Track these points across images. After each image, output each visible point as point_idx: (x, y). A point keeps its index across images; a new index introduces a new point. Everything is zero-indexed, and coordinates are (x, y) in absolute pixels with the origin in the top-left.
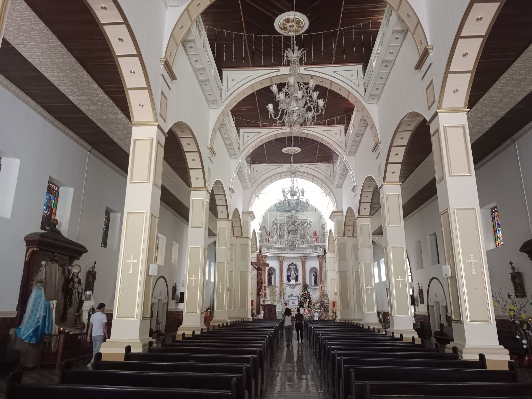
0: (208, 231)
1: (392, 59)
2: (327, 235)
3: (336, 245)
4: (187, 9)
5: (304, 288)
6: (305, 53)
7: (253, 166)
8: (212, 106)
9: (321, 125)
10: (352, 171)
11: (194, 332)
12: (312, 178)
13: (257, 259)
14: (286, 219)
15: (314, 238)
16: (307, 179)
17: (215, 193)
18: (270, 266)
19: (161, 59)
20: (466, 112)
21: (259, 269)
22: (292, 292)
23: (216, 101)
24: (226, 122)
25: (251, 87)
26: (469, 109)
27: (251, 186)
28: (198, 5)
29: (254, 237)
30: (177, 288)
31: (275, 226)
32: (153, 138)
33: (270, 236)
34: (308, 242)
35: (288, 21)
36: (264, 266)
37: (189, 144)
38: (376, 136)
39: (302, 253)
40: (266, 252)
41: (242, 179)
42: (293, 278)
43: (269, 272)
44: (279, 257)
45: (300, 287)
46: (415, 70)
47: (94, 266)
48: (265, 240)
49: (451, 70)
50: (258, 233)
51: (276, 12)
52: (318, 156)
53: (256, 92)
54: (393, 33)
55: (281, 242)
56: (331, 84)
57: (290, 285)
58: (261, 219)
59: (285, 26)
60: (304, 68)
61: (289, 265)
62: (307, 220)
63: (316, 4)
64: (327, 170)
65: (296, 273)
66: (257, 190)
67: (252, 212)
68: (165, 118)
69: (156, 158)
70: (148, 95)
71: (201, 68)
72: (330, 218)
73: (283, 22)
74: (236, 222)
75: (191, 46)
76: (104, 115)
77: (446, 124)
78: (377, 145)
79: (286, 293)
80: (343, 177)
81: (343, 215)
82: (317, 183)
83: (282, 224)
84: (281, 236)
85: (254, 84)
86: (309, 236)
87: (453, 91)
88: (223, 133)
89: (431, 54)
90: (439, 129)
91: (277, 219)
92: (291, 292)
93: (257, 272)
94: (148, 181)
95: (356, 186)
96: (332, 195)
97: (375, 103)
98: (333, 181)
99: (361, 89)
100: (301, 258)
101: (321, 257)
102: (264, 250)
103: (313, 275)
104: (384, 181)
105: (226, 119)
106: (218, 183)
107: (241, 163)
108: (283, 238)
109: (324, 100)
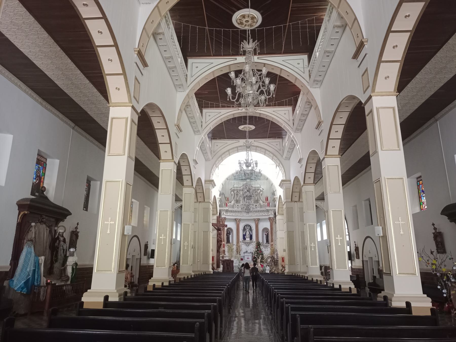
1: (333, 50)
2: (277, 200)
4: (157, 6)
5: (257, 246)
6: (259, 44)
7: (214, 141)
8: (179, 90)
9: (272, 106)
10: (299, 146)
11: (163, 283)
14: (242, 186)
15: (266, 203)
16: (260, 153)
18: (228, 227)
19: (135, 49)
20: (396, 95)
21: (219, 230)
23: (182, 85)
25: (212, 73)
28: (167, 3)
29: (215, 202)
30: (148, 246)
31: (232, 193)
33: (228, 201)
35: (244, 16)
37: (159, 122)
38: (319, 116)
39: (256, 215)
40: (224, 215)
42: (248, 237)
43: (227, 232)
44: (236, 219)
46: (352, 59)
47: (77, 227)
48: (224, 205)
50: (218, 198)
55: (238, 206)
57: (245, 243)
59: (242, 21)
60: (258, 58)
61: (245, 226)
62: (260, 187)
65: (251, 233)
66: (217, 162)
67: (213, 180)
68: (138, 100)
72: (280, 185)
73: (240, 18)
74: (199, 189)
77: (378, 106)
78: (319, 123)
79: (242, 250)
81: (290, 183)
82: (269, 156)
83: (239, 191)
86: (262, 201)
88: (188, 113)
89: (366, 46)
90: (373, 110)
91: (234, 186)
92: (246, 249)
93: (218, 232)
96: (281, 166)
98: (282, 154)
99: (306, 76)
102: (223, 213)
103: (265, 235)
105: (191, 101)
106: (184, 156)
107: (204, 138)
108: (240, 203)
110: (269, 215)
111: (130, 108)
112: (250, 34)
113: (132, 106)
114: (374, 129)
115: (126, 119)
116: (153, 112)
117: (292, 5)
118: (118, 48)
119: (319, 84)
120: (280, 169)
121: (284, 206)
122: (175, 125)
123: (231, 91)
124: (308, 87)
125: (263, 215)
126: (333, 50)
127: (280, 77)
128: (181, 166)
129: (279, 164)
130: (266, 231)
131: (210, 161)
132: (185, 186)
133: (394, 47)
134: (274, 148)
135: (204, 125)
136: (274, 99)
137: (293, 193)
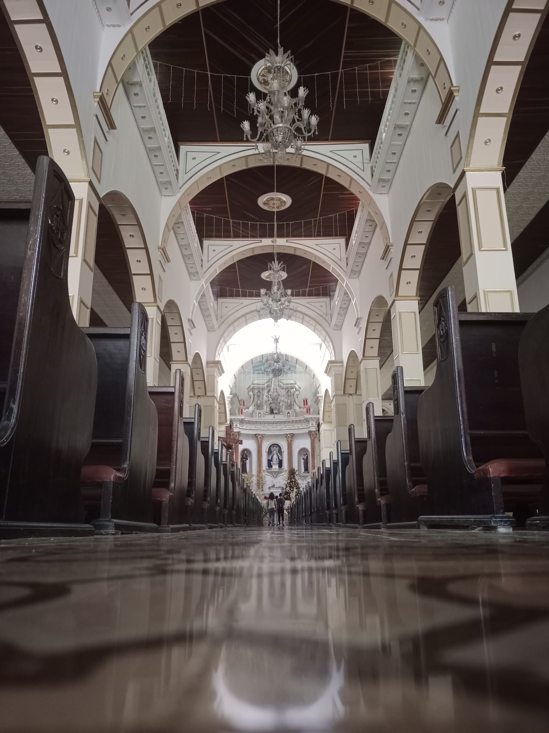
0: (158, 363)
1: (407, 123)
2: (321, 401)
3: (334, 406)
4: (130, 31)
6: (293, 58)
7: (221, 300)
8: (165, 192)
9: (314, 236)
12: (302, 318)
13: (227, 434)
14: (266, 382)
15: (305, 409)
17: (168, 323)
19: (94, 94)
20: (501, 170)
22: (274, 482)
23: (170, 183)
24: (184, 219)
25: (218, 168)
26: (504, 167)
27: (219, 327)
28: (146, 29)
29: (222, 403)
31: (251, 393)
32: (83, 198)
33: (244, 405)
34: (297, 415)
35: (272, 199)
36: (236, 443)
37: (133, 236)
40: (238, 428)
41: (206, 314)
42: (276, 463)
43: (242, 456)
44: (257, 434)
45: (285, 475)
46: (436, 125)
48: (237, 412)
49: (482, 111)
50: (228, 398)
51: (253, 56)
52: (309, 286)
53: (226, 179)
54: (409, 82)
56: (328, 168)
58: (233, 380)
59: (265, 78)
60: (287, 240)
61: (270, 446)
62: (296, 384)
63: (307, 46)
64: (321, 306)
65: (280, 457)
66: (227, 333)
67: (220, 361)
69: (84, 245)
70: (76, 136)
71: (150, 128)
73: (263, 72)
74: (198, 374)
75: (136, 92)
76: (11, 184)
77: (475, 186)
79: (265, 483)
80: (343, 313)
81: (342, 366)
82: (309, 324)
83: (261, 391)
84: (259, 407)
85: (222, 164)
87: (484, 142)
88: (180, 237)
89: (456, 98)
90: (467, 193)
91: (254, 383)
92: (272, 482)
93: (227, 451)
94: (75, 255)
95: (361, 319)
97: (385, 193)
98: (329, 321)
99: (367, 174)
100: (286, 436)
101: (313, 434)
102: (236, 425)
103: (303, 459)
104: (397, 295)
105: (184, 215)
106: (171, 305)
107: (205, 287)
108: (262, 409)
109: (317, 116)
110: (308, 427)
111: (87, 184)
112: (279, 44)
113: (89, 182)
114: (468, 211)
115: (79, 202)
116: (123, 215)
117: (344, 53)
118: (68, 79)
119: (387, 186)
120: (327, 347)
121: (332, 404)
122: (159, 248)
123: (249, 126)
124: (369, 193)
125: (300, 428)
126: (408, 124)
127: (328, 180)
128: (169, 327)
129: (325, 338)
130: (305, 453)
131: (214, 331)
132: (174, 361)
133: (497, 91)
134: (319, 313)
135: (206, 265)
136: (317, 223)
137: (347, 380)
